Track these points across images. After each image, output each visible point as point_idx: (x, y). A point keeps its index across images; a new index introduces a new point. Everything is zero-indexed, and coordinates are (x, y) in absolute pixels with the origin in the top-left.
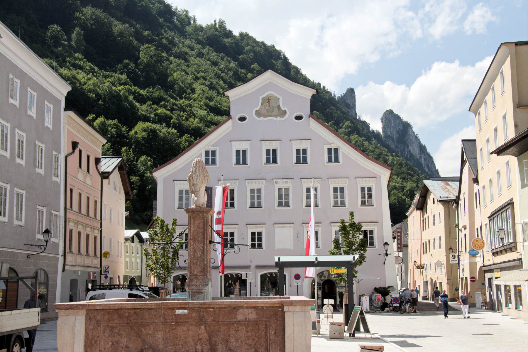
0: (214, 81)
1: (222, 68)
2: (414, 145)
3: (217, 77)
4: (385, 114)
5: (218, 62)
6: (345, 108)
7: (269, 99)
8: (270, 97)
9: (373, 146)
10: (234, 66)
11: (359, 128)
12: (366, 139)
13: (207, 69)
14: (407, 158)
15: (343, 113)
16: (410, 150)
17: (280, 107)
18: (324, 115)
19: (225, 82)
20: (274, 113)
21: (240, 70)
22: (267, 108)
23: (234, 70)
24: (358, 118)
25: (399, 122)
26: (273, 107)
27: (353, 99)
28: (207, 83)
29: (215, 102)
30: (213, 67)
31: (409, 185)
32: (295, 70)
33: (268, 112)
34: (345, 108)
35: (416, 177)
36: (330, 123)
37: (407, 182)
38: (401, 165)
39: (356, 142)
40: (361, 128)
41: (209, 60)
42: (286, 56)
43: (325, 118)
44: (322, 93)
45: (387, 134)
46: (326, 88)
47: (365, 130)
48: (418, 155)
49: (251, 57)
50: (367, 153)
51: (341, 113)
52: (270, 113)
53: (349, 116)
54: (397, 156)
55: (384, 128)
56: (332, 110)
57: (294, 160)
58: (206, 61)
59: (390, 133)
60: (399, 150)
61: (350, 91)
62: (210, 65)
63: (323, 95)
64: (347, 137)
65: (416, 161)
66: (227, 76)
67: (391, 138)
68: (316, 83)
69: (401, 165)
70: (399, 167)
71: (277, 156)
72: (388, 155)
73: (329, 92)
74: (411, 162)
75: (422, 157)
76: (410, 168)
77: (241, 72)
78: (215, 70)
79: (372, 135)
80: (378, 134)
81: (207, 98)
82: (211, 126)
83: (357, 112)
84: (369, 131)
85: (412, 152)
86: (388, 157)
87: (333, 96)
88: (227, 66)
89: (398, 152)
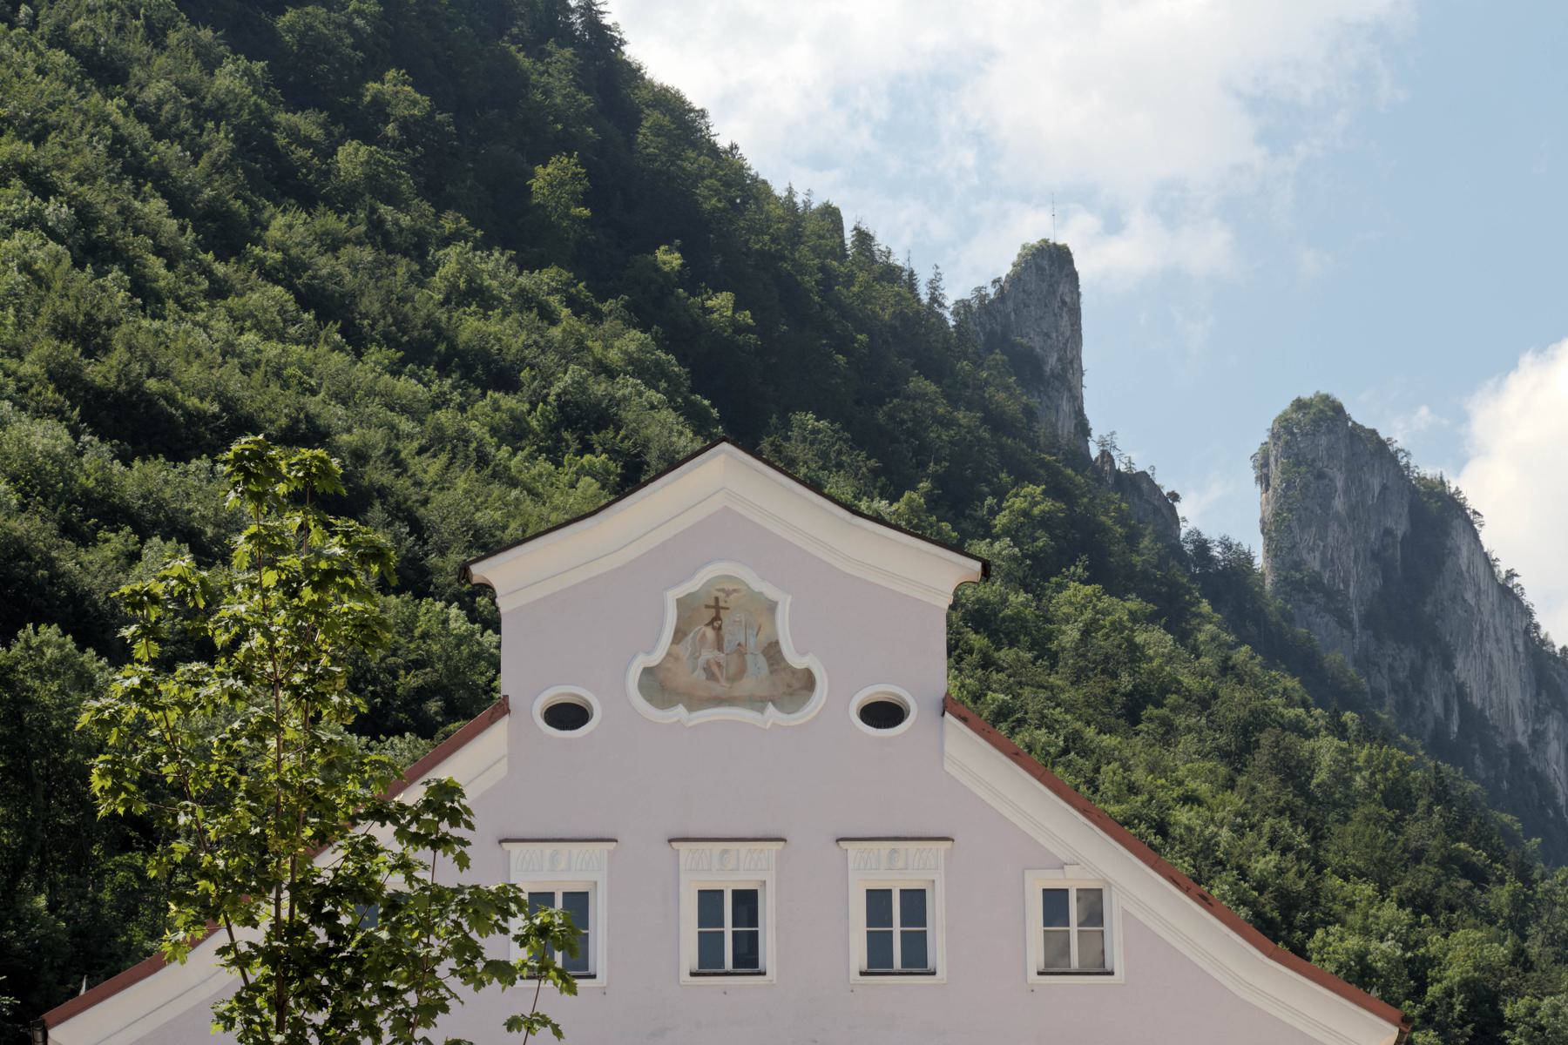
0: (102, 198)
1: (160, 103)
2: (1490, 646)
3: (126, 169)
4: (1285, 429)
5: (128, 60)
6: (1007, 388)
7: (717, 607)
8: (721, 595)
9: (1205, 660)
10: (241, 87)
11: (1104, 530)
12: (1151, 607)
13: (52, 107)
14: (1439, 745)
15: (997, 422)
16: (1461, 687)
17: (780, 652)
18: (863, 436)
19: (178, 208)
20: (747, 685)
21: (282, 117)
22: (708, 654)
23: (245, 116)
24: (1095, 452)
25: (1384, 488)
26: (741, 650)
27: (1065, 322)
28: (55, 211)
29: (126, 357)
30: (96, 97)
31: (1460, 951)
32: (666, 121)
33: (711, 676)
34: (1007, 388)
35: (1508, 887)
36: (911, 500)
37: (1450, 928)
38: (1399, 798)
39: (1086, 633)
40: (1119, 530)
41: (60, 39)
42: (607, 20)
43: (873, 463)
44: (850, 280)
45: (1297, 566)
46: (881, 242)
47: (1145, 543)
48: (1519, 723)
49: (359, 22)
50: (1165, 711)
51: (984, 421)
52: (721, 688)
53: (1034, 445)
54: (1370, 732)
55: (1274, 530)
56: (918, 405)
57: (859, 954)
58: (41, 46)
59: (1324, 565)
60: (1384, 684)
61: (1045, 263)
62: (69, 82)
63: (857, 295)
64: (1022, 597)
65: (1507, 761)
66: (196, 163)
67: (1330, 594)
68: (807, 204)
69: (1399, 798)
70: (1390, 815)
71: (760, 929)
72: (1310, 723)
73: (902, 270)
74: (1470, 773)
75: (1551, 735)
76: (1464, 822)
77: (295, 136)
78: (104, 119)
79: (1194, 578)
80: (1240, 565)
81: (64, 330)
82: (101, 534)
83: (1086, 412)
84: (1176, 549)
85: (1476, 701)
86: (1309, 744)
87: (925, 299)
88: (190, 90)
89: (1378, 696)
